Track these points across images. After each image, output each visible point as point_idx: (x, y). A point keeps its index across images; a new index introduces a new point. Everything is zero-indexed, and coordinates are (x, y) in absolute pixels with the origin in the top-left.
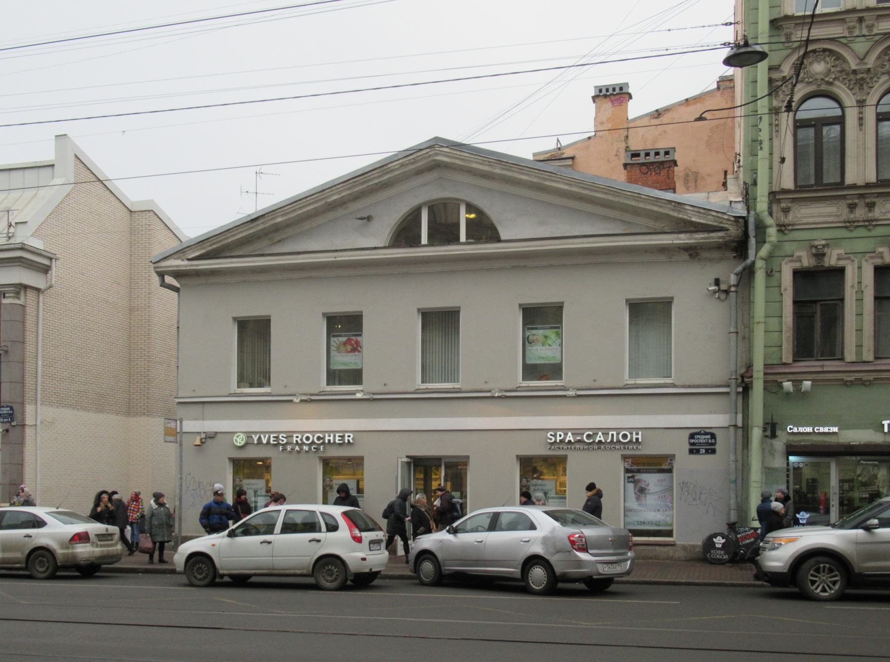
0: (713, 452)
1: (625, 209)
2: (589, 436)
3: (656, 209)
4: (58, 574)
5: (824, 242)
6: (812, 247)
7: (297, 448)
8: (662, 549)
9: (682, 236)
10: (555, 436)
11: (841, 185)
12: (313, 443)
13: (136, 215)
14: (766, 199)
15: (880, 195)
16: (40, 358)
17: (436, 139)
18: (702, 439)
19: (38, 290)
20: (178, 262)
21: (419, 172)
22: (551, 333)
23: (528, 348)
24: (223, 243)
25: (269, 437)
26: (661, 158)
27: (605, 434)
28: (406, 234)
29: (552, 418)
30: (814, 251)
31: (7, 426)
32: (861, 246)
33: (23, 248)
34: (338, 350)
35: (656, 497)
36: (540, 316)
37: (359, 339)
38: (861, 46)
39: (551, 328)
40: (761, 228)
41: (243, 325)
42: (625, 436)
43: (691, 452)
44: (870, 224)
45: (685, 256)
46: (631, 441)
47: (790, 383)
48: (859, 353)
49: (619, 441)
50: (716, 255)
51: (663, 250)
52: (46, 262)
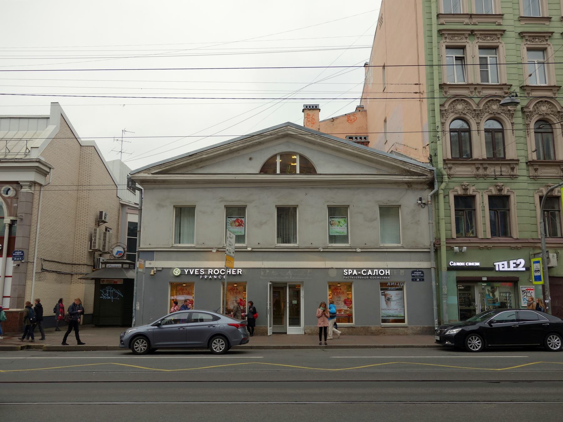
0: (423, 280)
1: (378, 162)
2: (364, 272)
3: (394, 164)
4: (230, 350)
5: (502, 184)
6: (462, 185)
7: (210, 277)
8: (401, 329)
9: (407, 177)
10: (348, 272)
11: (504, 159)
12: (219, 274)
13: (84, 148)
14: (442, 162)
15: (489, 164)
16: (39, 224)
17: (288, 122)
18: (418, 274)
19: (41, 185)
20: (146, 175)
21: (277, 138)
22: (342, 220)
23: (330, 227)
24: (172, 166)
25: (194, 271)
26: (363, 140)
27: (373, 272)
29: (211, 262)
30: (464, 187)
31: (19, 262)
32: (482, 186)
33: (39, 161)
34: (231, 225)
35: (395, 302)
36: (336, 211)
37: (243, 219)
38: (477, 100)
40: (441, 176)
42: (382, 272)
43: (413, 280)
44: (485, 176)
45: (406, 186)
46: (385, 275)
47: (465, 248)
48: (485, 235)
49: (379, 275)
50: (420, 187)
51: (396, 183)
52: (48, 170)
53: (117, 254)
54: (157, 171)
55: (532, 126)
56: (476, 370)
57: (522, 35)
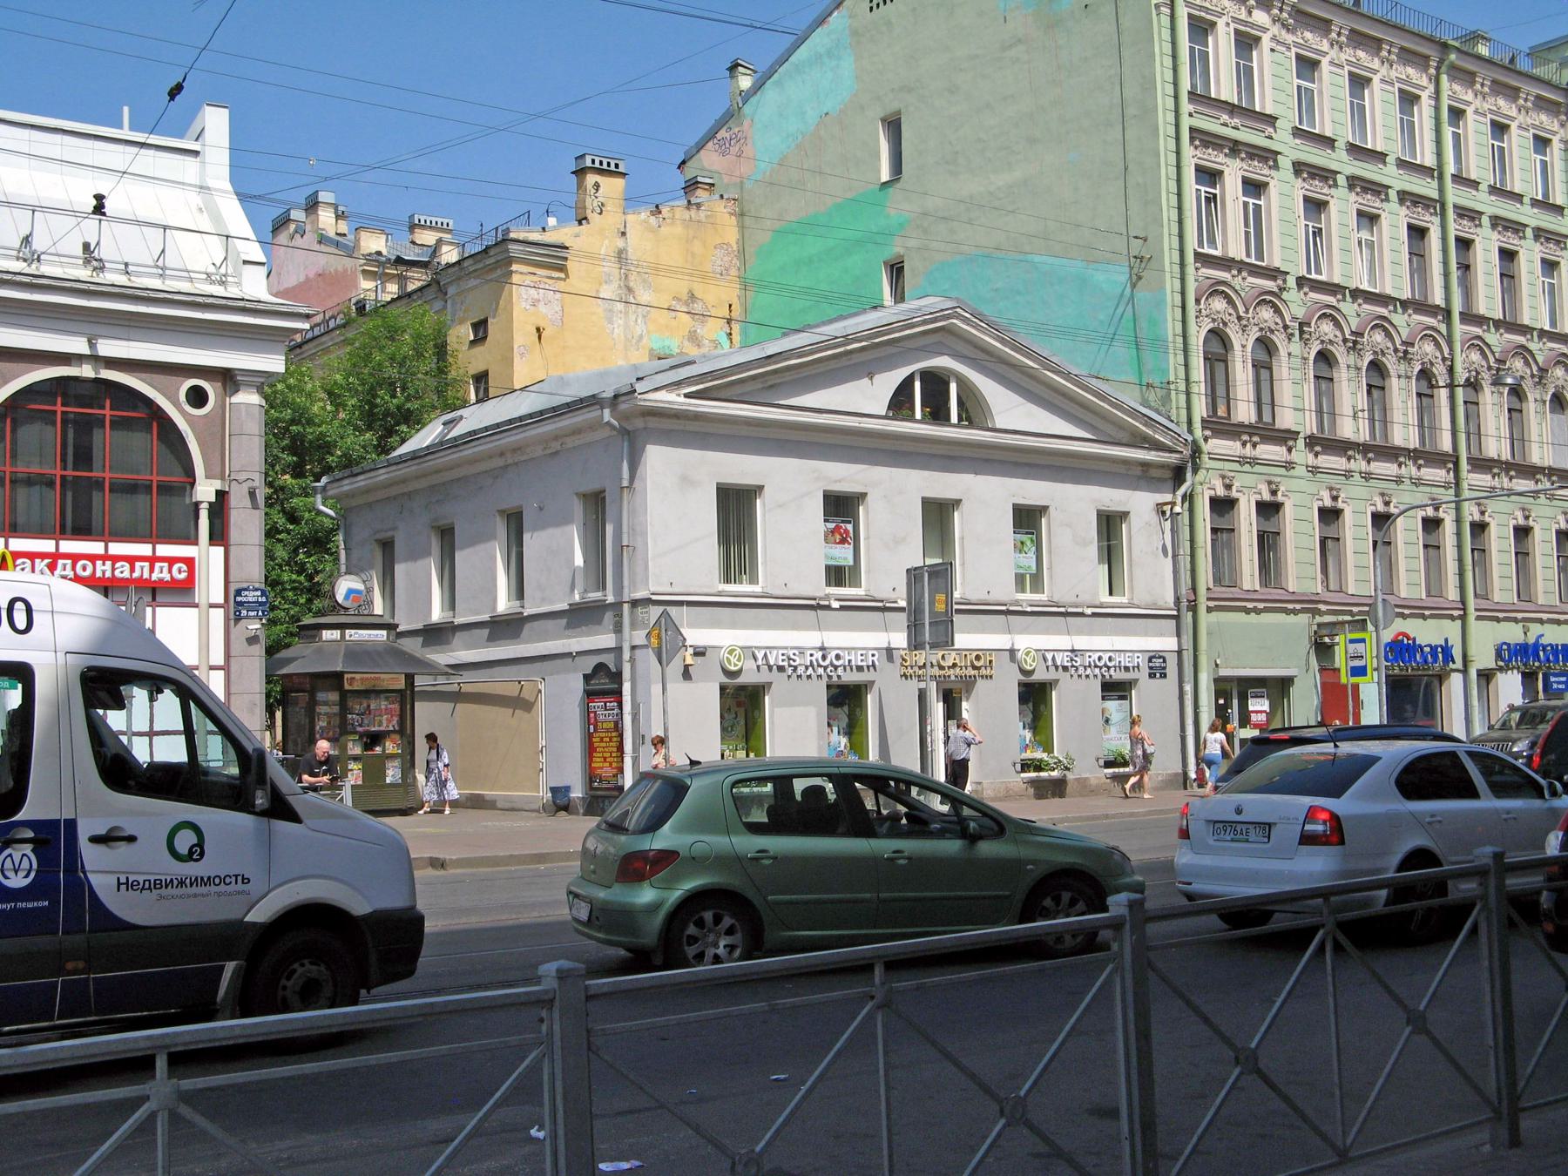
28: (900, 402)
41: (926, 503)
56: (149, 1037)
57: (1299, 168)
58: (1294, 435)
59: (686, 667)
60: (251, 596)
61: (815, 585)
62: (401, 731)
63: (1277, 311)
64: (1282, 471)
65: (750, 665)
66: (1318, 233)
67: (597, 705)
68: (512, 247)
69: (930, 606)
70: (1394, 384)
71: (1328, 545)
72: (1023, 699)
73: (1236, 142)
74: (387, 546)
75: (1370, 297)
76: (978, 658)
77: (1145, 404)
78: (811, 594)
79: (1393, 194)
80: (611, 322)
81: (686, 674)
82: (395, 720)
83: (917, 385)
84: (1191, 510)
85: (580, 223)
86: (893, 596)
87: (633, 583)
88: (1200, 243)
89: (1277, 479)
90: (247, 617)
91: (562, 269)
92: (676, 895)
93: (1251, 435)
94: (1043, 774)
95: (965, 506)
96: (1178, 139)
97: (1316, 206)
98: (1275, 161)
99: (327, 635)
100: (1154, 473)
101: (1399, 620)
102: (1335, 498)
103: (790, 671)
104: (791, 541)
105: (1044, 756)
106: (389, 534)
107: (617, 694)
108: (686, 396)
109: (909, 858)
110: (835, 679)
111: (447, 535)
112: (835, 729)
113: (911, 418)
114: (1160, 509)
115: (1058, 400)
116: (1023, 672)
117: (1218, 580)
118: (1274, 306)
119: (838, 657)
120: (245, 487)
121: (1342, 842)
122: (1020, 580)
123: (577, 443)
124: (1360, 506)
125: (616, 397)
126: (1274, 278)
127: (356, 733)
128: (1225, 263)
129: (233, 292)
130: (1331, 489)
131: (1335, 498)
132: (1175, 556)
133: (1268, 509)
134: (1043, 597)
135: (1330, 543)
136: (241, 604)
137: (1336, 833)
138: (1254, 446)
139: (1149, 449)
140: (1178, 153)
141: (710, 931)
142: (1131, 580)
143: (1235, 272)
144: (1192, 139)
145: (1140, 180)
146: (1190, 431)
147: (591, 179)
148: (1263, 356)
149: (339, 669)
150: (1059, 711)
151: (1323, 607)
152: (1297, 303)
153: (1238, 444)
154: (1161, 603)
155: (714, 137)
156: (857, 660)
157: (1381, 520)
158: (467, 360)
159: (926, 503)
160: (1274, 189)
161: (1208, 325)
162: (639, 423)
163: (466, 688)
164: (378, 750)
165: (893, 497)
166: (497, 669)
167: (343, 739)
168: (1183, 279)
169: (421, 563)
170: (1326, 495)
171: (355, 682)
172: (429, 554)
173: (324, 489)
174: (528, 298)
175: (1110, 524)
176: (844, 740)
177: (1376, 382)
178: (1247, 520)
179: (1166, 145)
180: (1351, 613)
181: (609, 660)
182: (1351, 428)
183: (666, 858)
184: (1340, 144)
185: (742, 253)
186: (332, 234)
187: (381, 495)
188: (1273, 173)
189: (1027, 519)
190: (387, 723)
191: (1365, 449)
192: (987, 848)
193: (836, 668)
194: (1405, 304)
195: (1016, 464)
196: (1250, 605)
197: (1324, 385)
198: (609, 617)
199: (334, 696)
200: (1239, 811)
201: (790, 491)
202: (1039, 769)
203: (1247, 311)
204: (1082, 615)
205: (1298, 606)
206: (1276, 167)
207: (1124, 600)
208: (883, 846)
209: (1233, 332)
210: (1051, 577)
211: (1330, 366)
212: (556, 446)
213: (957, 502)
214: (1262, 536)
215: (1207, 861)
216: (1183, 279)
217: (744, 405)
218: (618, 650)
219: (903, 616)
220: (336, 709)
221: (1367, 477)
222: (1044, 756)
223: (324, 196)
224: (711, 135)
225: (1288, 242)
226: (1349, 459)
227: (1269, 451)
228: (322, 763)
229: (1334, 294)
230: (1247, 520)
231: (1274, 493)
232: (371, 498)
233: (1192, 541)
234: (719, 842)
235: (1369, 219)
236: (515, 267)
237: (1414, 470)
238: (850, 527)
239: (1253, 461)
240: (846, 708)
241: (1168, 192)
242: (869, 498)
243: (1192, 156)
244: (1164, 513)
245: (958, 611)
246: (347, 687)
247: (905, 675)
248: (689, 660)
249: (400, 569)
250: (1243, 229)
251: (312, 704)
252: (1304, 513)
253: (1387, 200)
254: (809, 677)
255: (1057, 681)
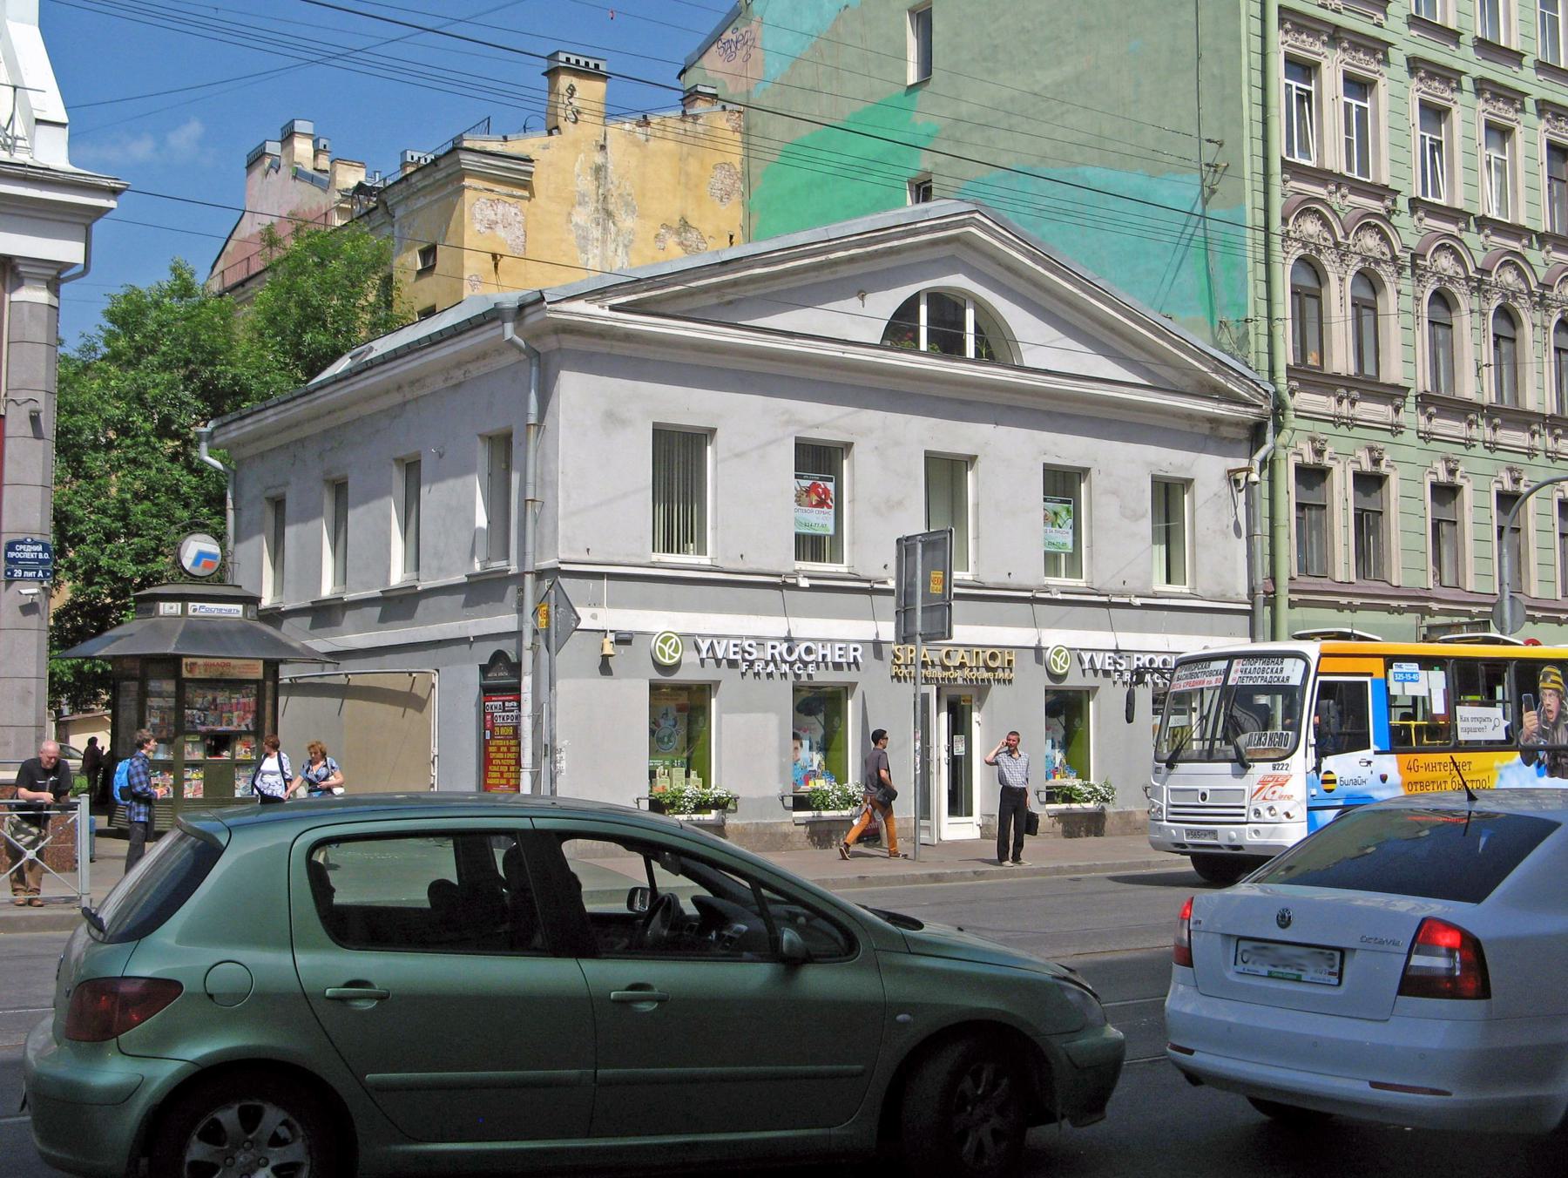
28: (900, 330)
39: (1062, 502)
41: (931, 459)
53: (196, 562)
54: (623, 300)
55: (1349, 280)
57: (1415, 65)
58: (1401, 391)
59: (605, 658)
60: (28, 552)
61: (780, 557)
62: (258, 733)
63: (1384, 238)
64: (1387, 436)
65: (691, 657)
66: (1437, 146)
67: (495, 703)
68: (466, 158)
69: (924, 587)
70: (1528, 333)
71: (1443, 530)
72: (1051, 711)
73: (1337, 28)
74: (278, 504)
75: (1500, 228)
76: (993, 656)
77: (1217, 345)
78: (775, 568)
79: (1530, 104)
80: (585, 251)
81: (605, 667)
82: (249, 719)
83: (923, 309)
84: (1272, 480)
85: (550, 133)
86: (883, 574)
87: (540, 550)
88: (1290, 151)
89: (1381, 446)
90: (22, 579)
91: (526, 185)
92: (163, 1072)
93: (1348, 389)
94: (1075, 806)
95: (981, 464)
96: (1264, 20)
97: (1434, 114)
98: (1386, 54)
99: (166, 608)
100: (1226, 431)
101: (1529, 624)
102: (1452, 472)
103: (744, 667)
104: (751, 501)
105: (1077, 783)
106: (280, 491)
107: (516, 690)
108: (612, 308)
109: (661, 1000)
110: (804, 678)
111: (340, 489)
112: (806, 743)
113: (915, 350)
114: (1232, 477)
115: (1105, 335)
116: (1053, 677)
117: (1304, 568)
118: (1381, 232)
119: (808, 651)
120: (25, 411)
121: (1484, 992)
122: (1051, 561)
123: (484, 370)
124: (1483, 483)
125: (522, 307)
126: (1381, 198)
127: (197, 733)
128: (1321, 176)
129: (20, 157)
130: (1447, 460)
131: (1452, 472)
132: (1250, 537)
133: (1368, 482)
134: (1080, 583)
135: (1444, 528)
136: (14, 561)
137: (1473, 974)
138: (1353, 403)
139: (1220, 401)
140: (1264, 37)
141: (237, 1146)
142: (1194, 565)
143: (1332, 188)
144: (1281, 22)
145: (1216, 70)
146: (1272, 380)
147: (565, 81)
148: (1365, 294)
149: (170, 650)
150: (1098, 728)
151: (1435, 606)
152: (1409, 231)
153: (1333, 399)
154: (1231, 595)
155: (718, 39)
156: (834, 656)
157: (1508, 501)
158: (412, 292)
159: (931, 459)
160: (1383, 89)
161: (1297, 251)
162: (551, 342)
163: (356, 681)
164: (226, 755)
165: (887, 453)
166: (389, 658)
167: (180, 739)
168: (1266, 193)
169: (312, 524)
170: (1441, 468)
171: (197, 667)
172: (320, 514)
173: (211, 436)
174: (483, 215)
175: (1168, 495)
176: (817, 758)
177: (1506, 331)
178: (1341, 493)
179: (1248, 26)
180: (1469, 614)
181: (508, 646)
182: (1473, 386)
183: (162, 991)
184: (1467, 39)
185: (746, 176)
186: (309, 168)
187: (273, 443)
188: (1382, 69)
189: (1062, 484)
190: (239, 721)
191: (1491, 413)
192: (820, 980)
193: (806, 664)
194: (1543, 238)
195: (1049, 413)
196: (1344, 600)
197: (1440, 332)
198: (512, 590)
199: (169, 686)
200: (1284, 921)
201: (751, 439)
202: (1068, 799)
203: (1346, 236)
204: (1129, 606)
205: (1404, 604)
206: (1386, 61)
207: (1185, 589)
208: (611, 974)
209: (1328, 261)
210: (1091, 557)
211: (1449, 309)
212: (458, 375)
213: (972, 459)
214: (1360, 516)
215: (1225, 1013)
216: (1266, 193)
217: (693, 322)
218: (518, 634)
219: (891, 602)
220: (172, 702)
221: (1492, 447)
222: (1077, 783)
223: (300, 126)
224: (715, 38)
225: (1400, 155)
226: (1470, 424)
227: (1368, 410)
228: (47, 773)
229: (1455, 221)
230: (1341, 493)
231: (1376, 462)
232: (263, 446)
233: (1272, 518)
234: (269, 963)
235: (1499, 133)
236: (467, 182)
237: (1550, 441)
238: (830, 486)
239: (1351, 423)
240: (821, 717)
241: (1250, 85)
242: (855, 449)
243: (1281, 45)
244: (1237, 482)
245: (959, 597)
246: (185, 674)
247: (897, 677)
248: (608, 650)
249: (290, 532)
250: (1343, 136)
251: (144, 694)
252: (1412, 489)
253: (1523, 110)
254: (770, 675)
255: (1096, 689)
